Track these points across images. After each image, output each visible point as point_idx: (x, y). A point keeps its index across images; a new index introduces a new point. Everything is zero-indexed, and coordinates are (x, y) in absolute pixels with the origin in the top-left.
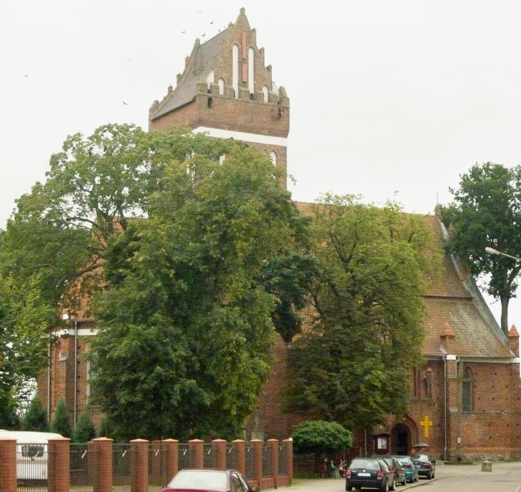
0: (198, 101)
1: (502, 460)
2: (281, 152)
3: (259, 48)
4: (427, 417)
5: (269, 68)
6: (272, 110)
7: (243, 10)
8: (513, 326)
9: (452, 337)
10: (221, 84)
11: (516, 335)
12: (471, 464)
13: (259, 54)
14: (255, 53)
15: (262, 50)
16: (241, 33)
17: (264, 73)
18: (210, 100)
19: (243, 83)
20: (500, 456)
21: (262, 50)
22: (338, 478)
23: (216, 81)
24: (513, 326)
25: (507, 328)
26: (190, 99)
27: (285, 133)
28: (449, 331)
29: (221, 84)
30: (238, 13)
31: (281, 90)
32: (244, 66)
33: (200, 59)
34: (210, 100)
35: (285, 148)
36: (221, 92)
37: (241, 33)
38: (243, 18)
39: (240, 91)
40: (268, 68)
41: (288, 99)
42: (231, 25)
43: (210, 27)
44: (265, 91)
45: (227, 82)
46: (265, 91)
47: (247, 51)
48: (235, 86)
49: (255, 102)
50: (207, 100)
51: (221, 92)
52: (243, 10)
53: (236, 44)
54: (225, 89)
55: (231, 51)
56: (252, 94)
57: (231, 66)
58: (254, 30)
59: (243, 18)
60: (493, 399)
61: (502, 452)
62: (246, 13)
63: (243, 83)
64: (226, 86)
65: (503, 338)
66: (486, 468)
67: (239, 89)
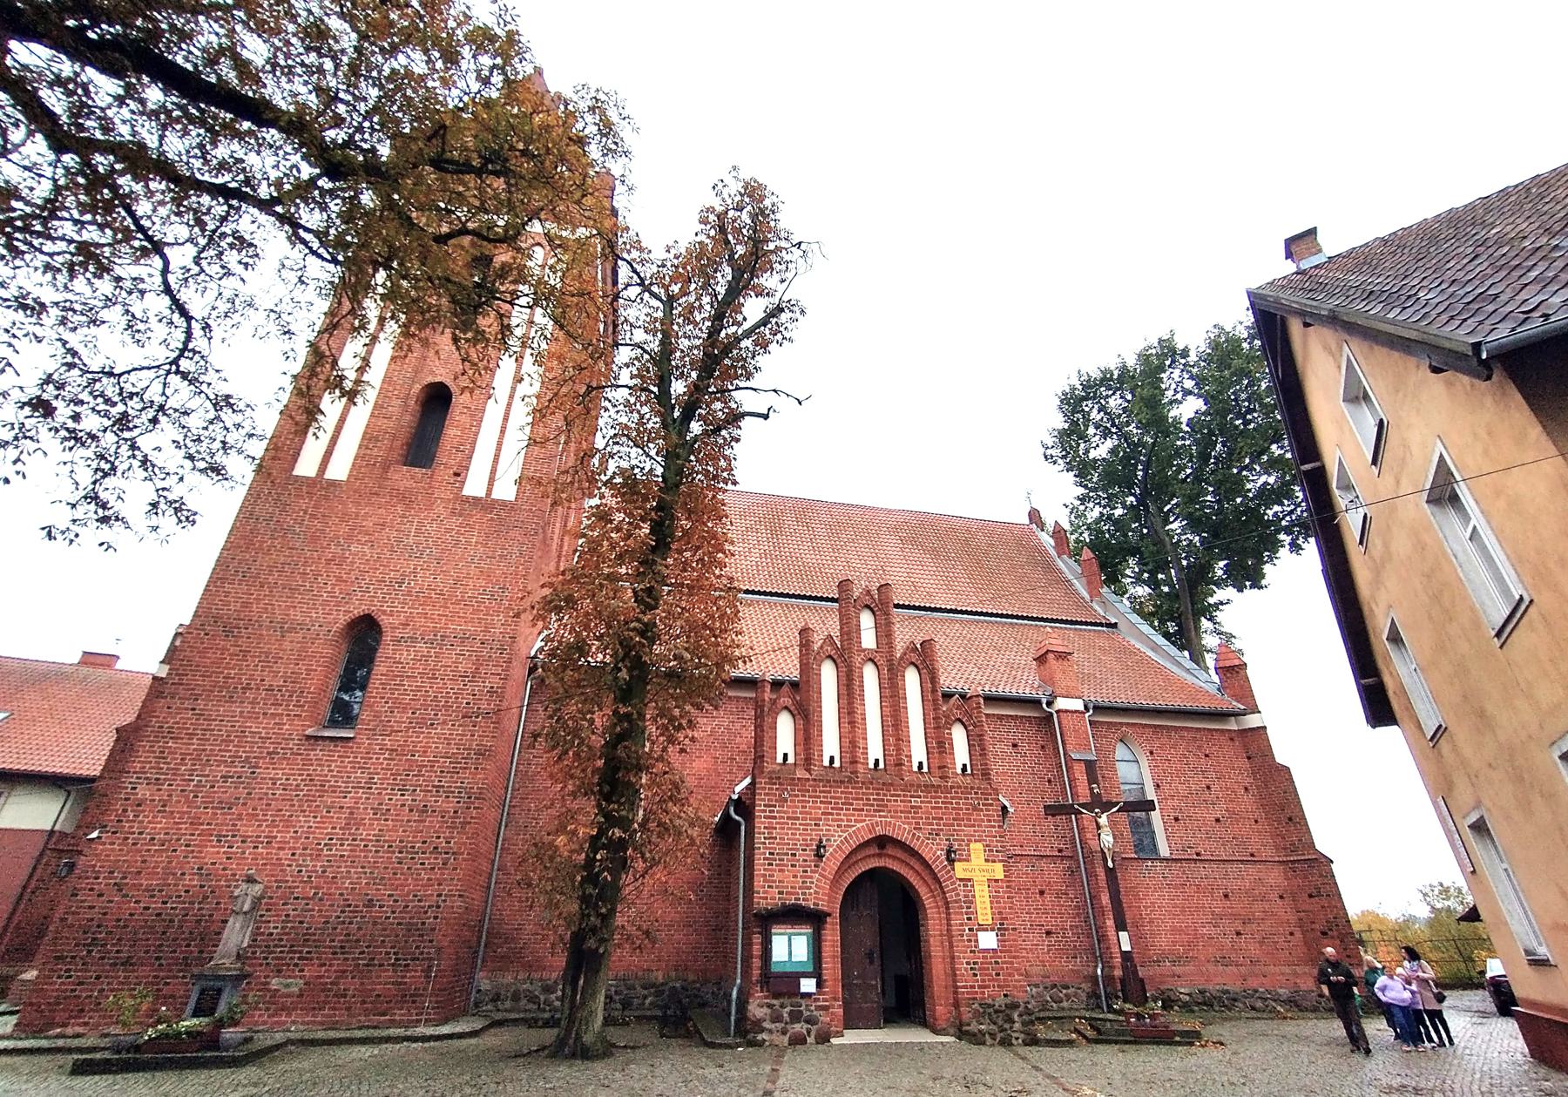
4: (979, 846)
11: (1237, 662)
60: (1218, 820)
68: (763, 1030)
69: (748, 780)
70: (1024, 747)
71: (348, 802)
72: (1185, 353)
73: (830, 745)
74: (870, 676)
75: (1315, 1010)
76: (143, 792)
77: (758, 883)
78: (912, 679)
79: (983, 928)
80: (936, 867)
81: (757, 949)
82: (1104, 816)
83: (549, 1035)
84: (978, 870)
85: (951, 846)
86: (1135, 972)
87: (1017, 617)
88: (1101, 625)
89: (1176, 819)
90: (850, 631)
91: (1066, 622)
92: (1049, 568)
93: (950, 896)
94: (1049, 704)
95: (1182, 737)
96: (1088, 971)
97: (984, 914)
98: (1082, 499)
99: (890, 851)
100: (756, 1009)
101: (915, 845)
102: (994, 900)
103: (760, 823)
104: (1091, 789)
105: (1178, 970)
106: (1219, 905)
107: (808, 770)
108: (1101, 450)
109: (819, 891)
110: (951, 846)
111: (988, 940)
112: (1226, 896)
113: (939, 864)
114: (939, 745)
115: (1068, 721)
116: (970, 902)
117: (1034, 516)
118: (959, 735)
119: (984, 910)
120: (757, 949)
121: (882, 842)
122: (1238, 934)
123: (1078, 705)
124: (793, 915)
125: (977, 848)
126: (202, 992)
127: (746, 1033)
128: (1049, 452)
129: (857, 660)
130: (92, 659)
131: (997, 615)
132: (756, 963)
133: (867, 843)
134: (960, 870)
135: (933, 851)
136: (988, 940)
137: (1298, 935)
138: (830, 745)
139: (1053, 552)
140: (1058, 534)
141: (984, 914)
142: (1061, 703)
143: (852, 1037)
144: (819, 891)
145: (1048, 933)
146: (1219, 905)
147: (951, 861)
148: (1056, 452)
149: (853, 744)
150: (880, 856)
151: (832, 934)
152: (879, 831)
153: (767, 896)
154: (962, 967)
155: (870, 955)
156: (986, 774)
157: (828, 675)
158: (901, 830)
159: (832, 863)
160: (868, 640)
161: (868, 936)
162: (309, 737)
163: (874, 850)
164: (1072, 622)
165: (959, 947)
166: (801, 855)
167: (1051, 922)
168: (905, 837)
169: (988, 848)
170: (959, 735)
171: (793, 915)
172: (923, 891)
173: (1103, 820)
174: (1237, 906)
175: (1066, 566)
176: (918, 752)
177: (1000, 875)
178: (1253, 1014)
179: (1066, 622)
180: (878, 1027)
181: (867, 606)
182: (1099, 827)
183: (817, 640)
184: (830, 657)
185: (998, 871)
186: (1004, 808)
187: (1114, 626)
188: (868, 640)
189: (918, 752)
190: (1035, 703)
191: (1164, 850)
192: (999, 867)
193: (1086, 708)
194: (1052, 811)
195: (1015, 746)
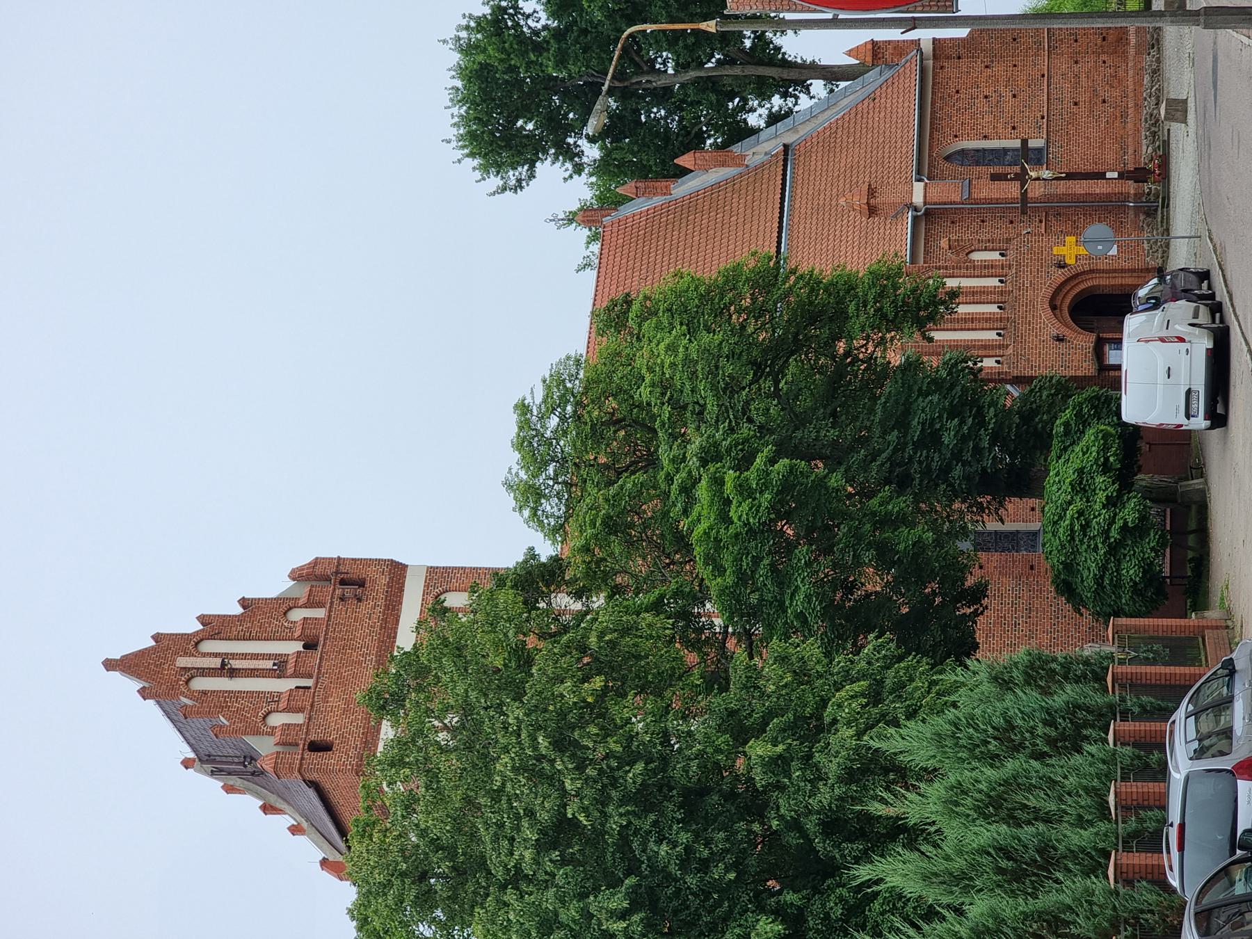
0: (314, 776)
1: (1156, 72)
2: (440, 578)
3: (238, 610)
4: (1055, 249)
5: (157, 637)
6: (342, 599)
7: (110, 665)
8: (849, 53)
9: (872, 192)
10: (277, 720)
11: (870, 47)
12: (1166, 144)
13: (214, 626)
14: (212, 637)
15: (203, 619)
16: (158, 669)
17: (257, 616)
18: (316, 747)
19: (280, 668)
20: (1147, 79)
21: (203, 619)
22: (1206, 483)
23: (272, 732)
24: (849, 53)
25: (851, 66)
26: (311, 793)
27: (397, 571)
28: (859, 200)
29: (277, 720)
30: (116, 675)
31: (298, 575)
32: (236, 664)
33: (227, 763)
34: (316, 747)
35: (432, 571)
36: (299, 719)
37: (158, 669)
38: (127, 665)
39: (296, 675)
40: (244, 608)
41: (317, 561)
42: (144, 694)
43: (156, 737)
44: (297, 615)
45: (274, 706)
46: (297, 615)
47: (204, 655)
48: (284, 685)
49: (322, 639)
50: (314, 755)
51: (299, 719)
52: (110, 665)
53: (187, 682)
54: (288, 710)
55: (205, 693)
56: (305, 647)
57: (237, 695)
58: (157, 637)
59: (127, 665)
60: (1014, 96)
61: (1139, 72)
62: (117, 656)
63: (280, 668)
64: (282, 705)
65: (873, 78)
66: (1178, 110)
67: (291, 676)
69: (1009, 387)
75: (1158, 61)
80: (1068, 274)
84: (1070, 250)
86: (1129, 172)
89: (1014, 128)
93: (1087, 268)
94: (916, 209)
96: (1131, 213)
101: (1054, 286)
104: (1012, 179)
105: (1131, 151)
106: (1083, 109)
107: (1007, 346)
109: (1085, 341)
112: (1076, 104)
113: (1067, 273)
114: (986, 269)
118: (977, 256)
125: (1056, 250)
128: (513, 182)
134: (1070, 261)
135: (1059, 276)
136: (1114, 251)
137: (1104, 57)
142: (918, 199)
146: (1083, 109)
148: (512, 176)
149: (987, 320)
152: (1046, 306)
154: (1126, 265)
158: (1045, 292)
159: (1067, 332)
163: (1057, 312)
165: (1116, 266)
168: (1051, 291)
170: (977, 256)
173: (1033, 174)
174: (1083, 98)
182: (1038, 179)
187: (786, 147)
192: (1068, 239)
194: (1024, 212)
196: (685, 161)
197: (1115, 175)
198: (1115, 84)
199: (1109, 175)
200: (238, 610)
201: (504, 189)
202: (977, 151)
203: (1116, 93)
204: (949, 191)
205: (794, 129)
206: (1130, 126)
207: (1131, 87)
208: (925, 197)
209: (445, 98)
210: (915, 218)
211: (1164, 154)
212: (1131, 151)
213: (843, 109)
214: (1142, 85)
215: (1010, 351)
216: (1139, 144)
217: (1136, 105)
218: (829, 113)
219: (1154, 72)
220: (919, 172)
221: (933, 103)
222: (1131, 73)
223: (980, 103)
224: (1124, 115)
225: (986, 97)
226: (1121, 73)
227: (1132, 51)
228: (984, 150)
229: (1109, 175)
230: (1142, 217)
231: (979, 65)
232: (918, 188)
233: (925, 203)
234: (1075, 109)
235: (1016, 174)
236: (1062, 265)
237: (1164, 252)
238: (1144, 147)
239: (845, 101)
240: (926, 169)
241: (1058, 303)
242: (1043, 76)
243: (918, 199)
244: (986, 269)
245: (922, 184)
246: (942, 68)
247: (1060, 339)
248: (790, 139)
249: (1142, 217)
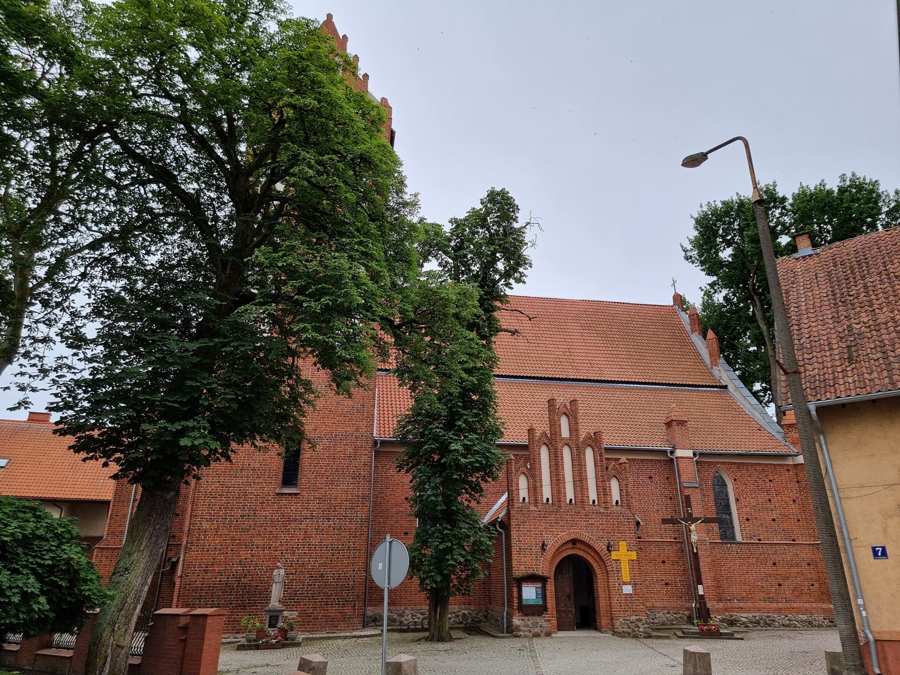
4: (624, 543)
9: (682, 423)
20: (804, 617)
60: (774, 520)
68: (520, 630)
70: (656, 478)
71: (303, 526)
72: (784, 199)
73: (547, 492)
74: (566, 453)
75: (820, 626)
76: (205, 525)
77: (514, 562)
78: (589, 454)
79: (625, 583)
81: (515, 594)
82: (693, 526)
83: (427, 634)
84: (624, 555)
85: (609, 544)
86: (705, 603)
87: (659, 384)
88: (716, 387)
90: (554, 426)
91: (692, 386)
92: (686, 342)
94: (672, 453)
95: (756, 470)
97: (626, 577)
98: (712, 285)
99: (578, 546)
100: (516, 621)
102: (632, 569)
103: (514, 534)
105: (741, 605)
106: (770, 569)
108: (726, 254)
109: (544, 567)
110: (609, 544)
111: (628, 589)
112: (774, 564)
114: (603, 491)
115: (682, 464)
116: (619, 571)
117: (679, 300)
118: (614, 485)
119: (626, 575)
120: (515, 594)
121: (574, 542)
122: (780, 585)
123: (690, 453)
124: (532, 578)
126: (270, 617)
127: (511, 631)
128: (689, 254)
129: (559, 445)
130: (36, 417)
131: (645, 383)
132: (516, 600)
133: (567, 542)
134: (614, 555)
135: (601, 546)
136: (628, 589)
137: (816, 585)
138: (547, 492)
139: (688, 328)
140: (694, 316)
141: (626, 577)
142: (679, 453)
143: (561, 634)
144: (544, 567)
145: (666, 584)
146: (770, 569)
147: (610, 551)
148: (695, 253)
149: (559, 491)
150: (573, 548)
151: (551, 587)
152: (573, 536)
153: (519, 570)
154: (615, 601)
155: (569, 596)
156: (629, 506)
157: (544, 453)
158: (585, 536)
160: (565, 433)
161: (568, 589)
162: (278, 494)
163: (570, 545)
164: (696, 386)
165: (613, 593)
166: (534, 551)
167: (667, 578)
168: (586, 540)
169: (629, 545)
170: (614, 485)
171: (532, 578)
172: (595, 565)
173: (693, 527)
174: (781, 571)
175: (696, 339)
176: (593, 495)
177: (635, 558)
178: (782, 628)
179: (692, 386)
180: (573, 630)
181: (565, 413)
183: (538, 434)
184: (545, 443)
185: (634, 555)
186: (638, 523)
187: (726, 387)
188: (565, 433)
189: (593, 495)
190: (664, 452)
191: (739, 538)
193: (694, 454)
195: (650, 478)
196: (711, 334)
197: (701, 592)
198: (796, 593)
199: (700, 587)
200: (361, 74)
201: (685, 251)
202: (727, 495)
203: (788, 594)
204: (688, 474)
205: (737, 388)
206: (762, 604)
207: (794, 605)
208: (682, 458)
209: (726, 198)
210: (665, 452)
211: (721, 634)
212: (741, 605)
213: (752, 414)
214: (798, 613)
215: (532, 508)
216: (749, 611)
217: (780, 609)
218: (749, 406)
219: (810, 623)
220: (701, 454)
221: (759, 464)
222: (807, 605)
223: (764, 496)
224: (770, 600)
225: (770, 500)
226: (805, 598)
227: (825, 606)
228: (728, 500)
229: (700, 587)
230: (687, 613)
231: (793, 495)
232: (690, 453)
233: (677, 458)
234: (770, 563)
235: (691, 514)
236: (609, 548)
237: (629, 634)
238: (745, 615)
239: (757, 414)
240: (703, 459)
241: (578, 546)
242: (794, 540)
243: (679, 453)
244: (603, 491)
245: (692, 455)
246: (788, 470)
247: (543, 547)
248: (730, 388)
249: (687, 613)
